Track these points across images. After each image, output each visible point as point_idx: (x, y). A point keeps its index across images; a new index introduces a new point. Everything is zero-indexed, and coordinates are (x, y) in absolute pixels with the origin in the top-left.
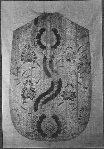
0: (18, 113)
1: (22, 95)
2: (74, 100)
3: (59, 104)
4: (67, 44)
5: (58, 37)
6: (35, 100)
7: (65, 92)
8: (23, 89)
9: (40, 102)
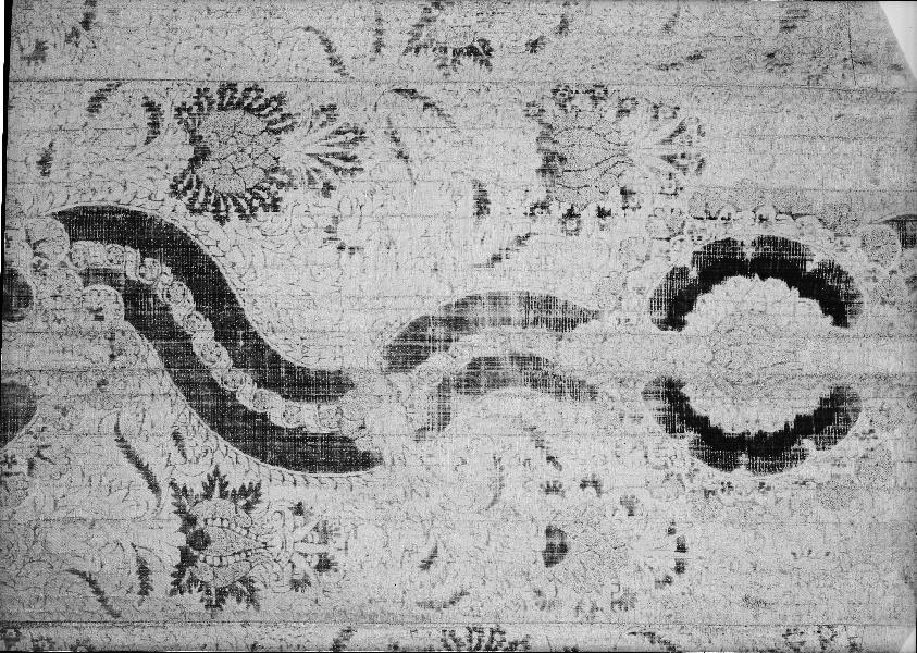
0: (50, 52)
1: (222, 93)
2: (178, 588)
3: (134, 445)
4: (711, 537)
5: (773, 450)
6: (172, 212)
7: (248, 507)
8: (280, 99)
9: (148, 261)
